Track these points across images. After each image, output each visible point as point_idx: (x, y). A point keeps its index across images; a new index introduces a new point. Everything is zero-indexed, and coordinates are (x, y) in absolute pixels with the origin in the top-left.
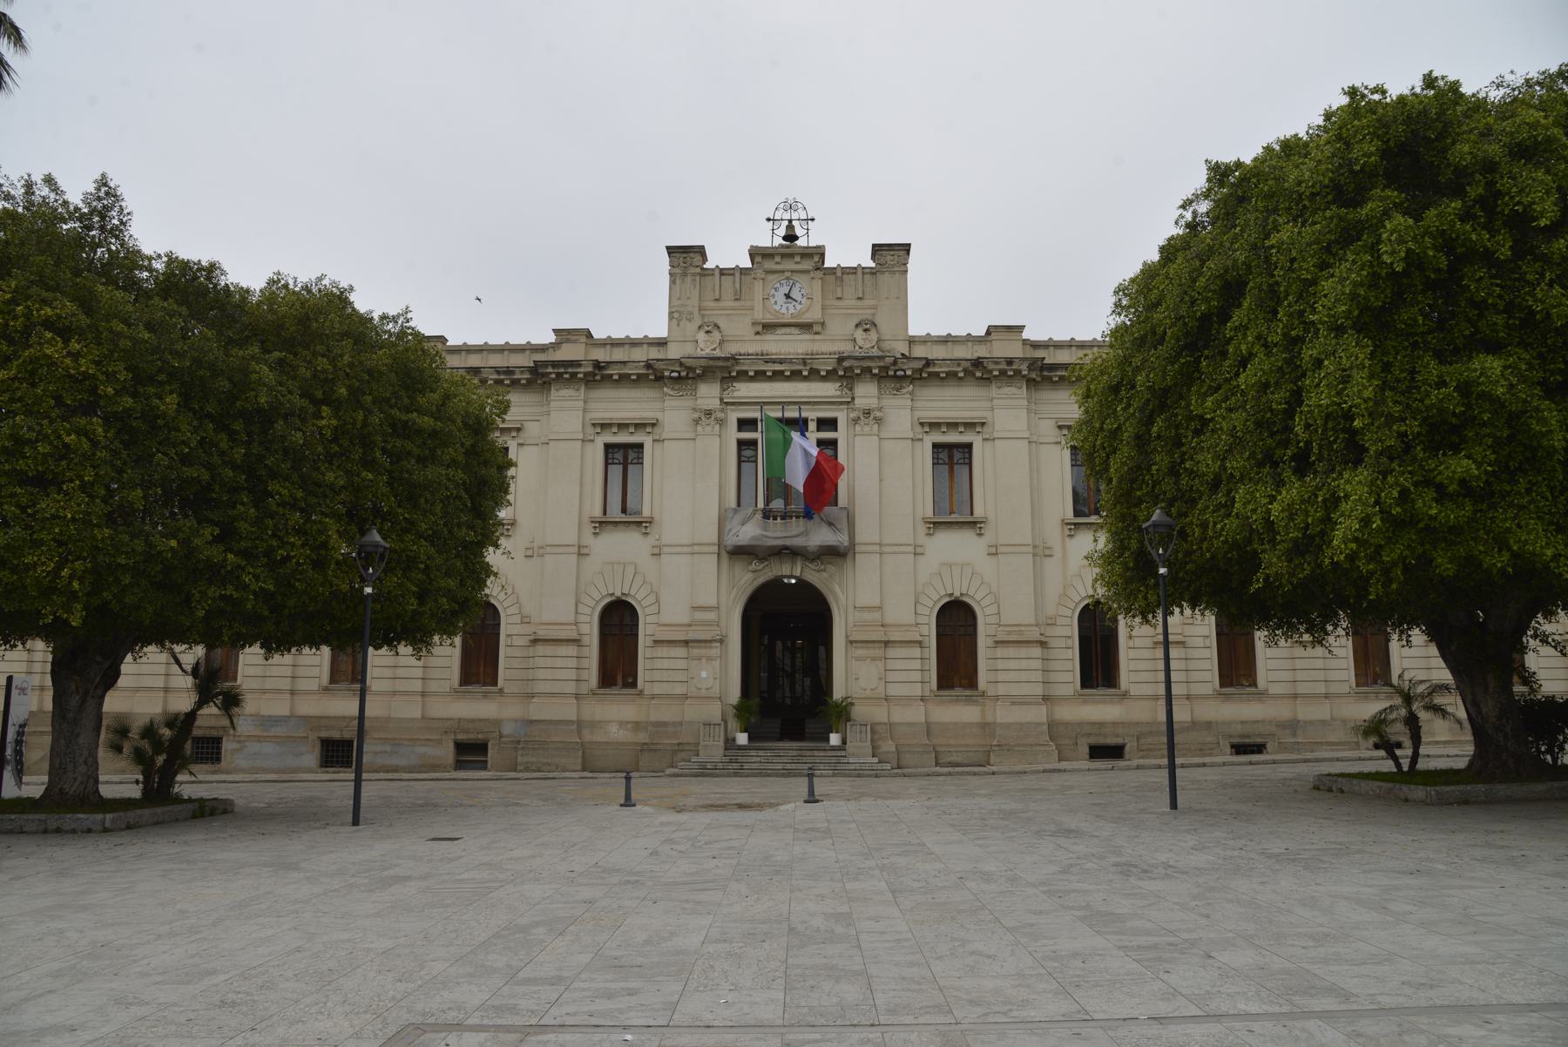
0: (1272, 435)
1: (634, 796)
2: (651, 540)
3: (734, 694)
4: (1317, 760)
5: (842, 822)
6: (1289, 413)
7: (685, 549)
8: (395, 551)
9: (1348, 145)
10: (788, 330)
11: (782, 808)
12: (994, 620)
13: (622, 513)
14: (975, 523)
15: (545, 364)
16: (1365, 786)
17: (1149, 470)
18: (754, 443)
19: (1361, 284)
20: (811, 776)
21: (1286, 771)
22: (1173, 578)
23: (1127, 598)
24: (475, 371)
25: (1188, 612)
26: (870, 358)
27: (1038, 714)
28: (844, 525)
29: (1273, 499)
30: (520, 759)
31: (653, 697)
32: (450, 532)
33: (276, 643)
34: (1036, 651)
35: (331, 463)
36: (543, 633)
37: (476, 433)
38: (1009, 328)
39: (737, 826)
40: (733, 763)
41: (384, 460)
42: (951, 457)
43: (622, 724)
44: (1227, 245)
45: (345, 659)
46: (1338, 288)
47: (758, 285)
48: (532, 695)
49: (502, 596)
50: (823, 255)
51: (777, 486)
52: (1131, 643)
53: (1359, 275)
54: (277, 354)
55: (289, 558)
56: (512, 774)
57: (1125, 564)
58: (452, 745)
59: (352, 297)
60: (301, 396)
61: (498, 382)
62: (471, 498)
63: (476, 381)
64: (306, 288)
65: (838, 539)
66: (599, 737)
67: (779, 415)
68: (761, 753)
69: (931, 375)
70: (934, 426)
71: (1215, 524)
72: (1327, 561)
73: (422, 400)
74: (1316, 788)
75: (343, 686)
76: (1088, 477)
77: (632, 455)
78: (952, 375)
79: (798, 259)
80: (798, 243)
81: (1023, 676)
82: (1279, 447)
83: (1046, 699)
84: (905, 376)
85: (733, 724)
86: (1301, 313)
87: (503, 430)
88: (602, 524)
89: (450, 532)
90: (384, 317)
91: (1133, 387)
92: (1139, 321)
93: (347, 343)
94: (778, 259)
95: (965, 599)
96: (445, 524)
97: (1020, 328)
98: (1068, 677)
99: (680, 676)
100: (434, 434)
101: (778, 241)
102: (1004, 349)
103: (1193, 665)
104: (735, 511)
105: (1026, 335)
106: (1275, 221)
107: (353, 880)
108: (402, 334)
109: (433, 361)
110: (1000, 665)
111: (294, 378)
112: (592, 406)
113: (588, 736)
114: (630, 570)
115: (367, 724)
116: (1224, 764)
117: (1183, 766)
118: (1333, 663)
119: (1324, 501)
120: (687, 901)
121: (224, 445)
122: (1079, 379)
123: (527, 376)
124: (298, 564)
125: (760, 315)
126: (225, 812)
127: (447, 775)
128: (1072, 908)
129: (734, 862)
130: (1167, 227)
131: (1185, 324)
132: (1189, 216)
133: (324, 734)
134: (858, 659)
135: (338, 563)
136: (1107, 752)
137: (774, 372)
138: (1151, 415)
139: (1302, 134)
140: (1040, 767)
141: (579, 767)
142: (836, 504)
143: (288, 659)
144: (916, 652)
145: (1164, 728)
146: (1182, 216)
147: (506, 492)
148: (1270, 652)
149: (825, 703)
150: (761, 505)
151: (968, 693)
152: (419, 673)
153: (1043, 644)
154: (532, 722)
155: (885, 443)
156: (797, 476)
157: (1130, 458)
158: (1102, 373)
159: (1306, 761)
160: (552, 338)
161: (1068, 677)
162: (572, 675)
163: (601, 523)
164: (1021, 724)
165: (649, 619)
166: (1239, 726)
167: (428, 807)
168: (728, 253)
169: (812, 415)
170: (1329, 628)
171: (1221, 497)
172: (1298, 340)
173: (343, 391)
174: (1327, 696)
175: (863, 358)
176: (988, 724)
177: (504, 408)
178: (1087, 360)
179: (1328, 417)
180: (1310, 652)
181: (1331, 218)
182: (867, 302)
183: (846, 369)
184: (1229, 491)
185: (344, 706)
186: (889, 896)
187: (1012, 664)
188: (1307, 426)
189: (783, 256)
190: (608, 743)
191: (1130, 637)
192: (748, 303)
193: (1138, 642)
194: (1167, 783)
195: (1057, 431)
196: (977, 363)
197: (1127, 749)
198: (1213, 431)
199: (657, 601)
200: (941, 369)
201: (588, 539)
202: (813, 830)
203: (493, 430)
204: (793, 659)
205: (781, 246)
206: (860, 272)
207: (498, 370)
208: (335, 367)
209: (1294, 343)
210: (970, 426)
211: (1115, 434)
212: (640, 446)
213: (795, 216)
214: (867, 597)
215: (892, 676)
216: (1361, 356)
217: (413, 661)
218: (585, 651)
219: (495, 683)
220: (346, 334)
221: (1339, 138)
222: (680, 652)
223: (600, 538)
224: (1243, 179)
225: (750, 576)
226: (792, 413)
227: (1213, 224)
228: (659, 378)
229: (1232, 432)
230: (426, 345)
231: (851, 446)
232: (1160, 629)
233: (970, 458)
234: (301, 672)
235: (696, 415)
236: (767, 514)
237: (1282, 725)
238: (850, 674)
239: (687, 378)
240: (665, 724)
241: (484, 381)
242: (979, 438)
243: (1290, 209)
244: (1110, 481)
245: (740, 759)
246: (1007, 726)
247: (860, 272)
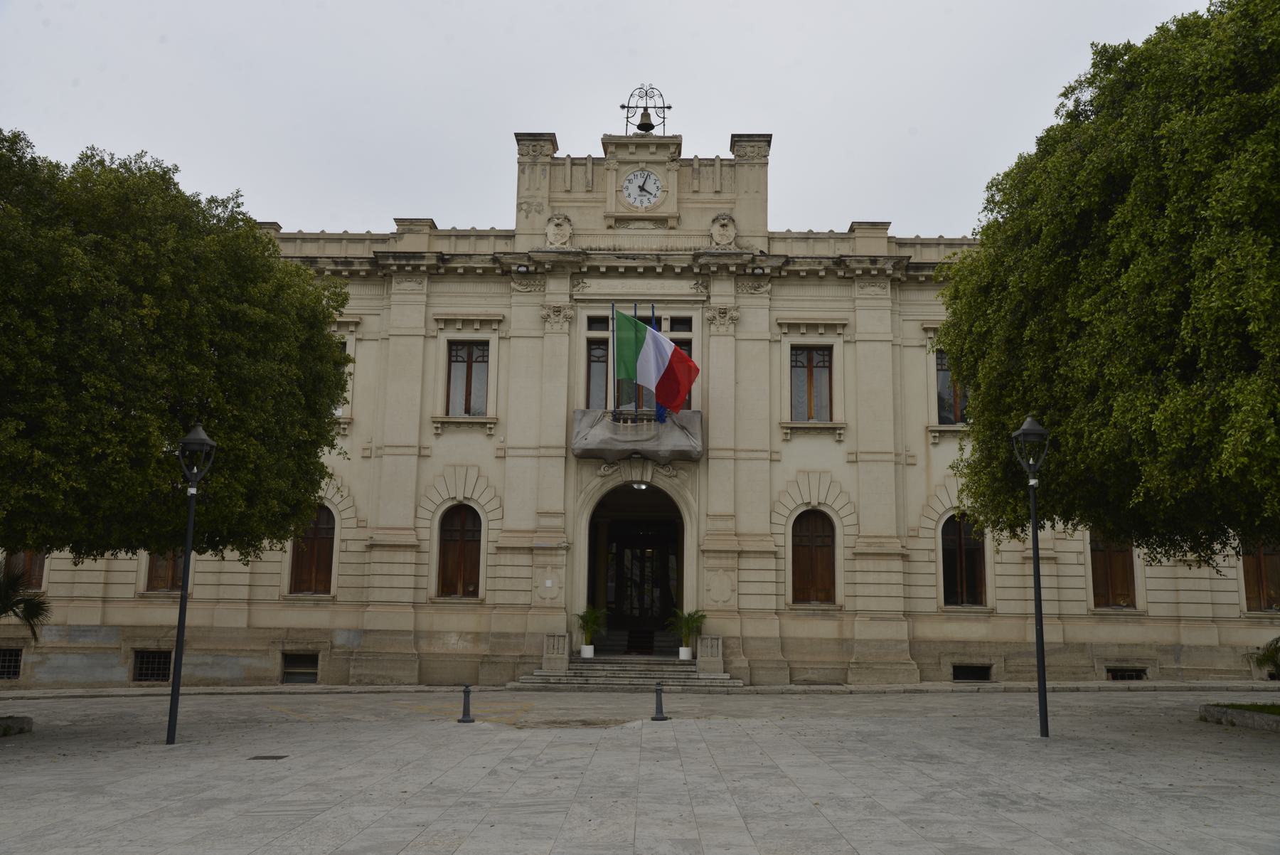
0: (1155, 339)
1: (473, 711)
2: (495, 442)
3: (581, 605)
4: (1203, 689)
5: (691, 741)
6: (1175, 317)
7: (531, 452)
8: (222, 450)
9: (1255, 22)
10: (641, 224)
11: (628, 725)
12: (853, 530)
13: (466, 414)
14: (835, 429)
15: (386, 255)
16: (1259, 719)
17: (1020, 375)
18: (604, 342)
19: (1262, 176)
20: (659, 692)
21: (1167, 700)
22: (1044, 489)
24: (311, 261)
25: (1060, 526)
27: (899, 631)
28: (697, 429)
29: (1154, 408)
30: (352, 671)
31: (495, 606)
32: (283, 430)
33: (85, 548)
34: (897, 565)
35: (152, 355)
36: (380, 538)
37: (312, 326)
38: (874, 225)
39: (581, 745)
40: (579, 676)
41: (212, 354)
42: (810, 360)
43: (461, 634)
44: (1112, 135)
46: (1232, 183)
47: (611, 176)
48: (367, 604)
49: (337, 499)
50: (679, 146)
51: (629, 389)
52: (998, 558)
53: (1259, 166)
54: (92, 236)
55: (104, 456)
57: (993, 474)
58: (279, 657)
59: (177, 178)
60: (120, 283)
61: (335, 273)
63: (312, 272)
64: (124, 165)
65: (689, 443)
66: (437, 649)
68: (607, 667)
69: (791, 273)
70: (793, 327)
71: (1091, 433)
72: (1214, 475)
73: (253, 291)
74: (1203, 719)
75: (163, 592)
76: (954, 382)
77: (476, 353)
78: (812, 274)
79: (653, 149)
81: (884, 590)
82: (1162, 352)
83: (908, 615)
84: (764, 275)
85: (578, 636)
86: (1192, 209)
87: (340, 324)
88: (444, 425)
89: (283, 430)
90: (212, 200)
91: (1005, 288)
92: (1013, 218)
93: (172, 227)
94: (632, 149)
95: (822, 508)
96: (277, 422)
97: (886, 225)
98: (931, 592)
99: (524, 585)
100: (266, 327)
101: (633, 130)
103: (1065, 582)
104: (584, 413)
105: (891, 232)
106: (1167, 108)
107: (165, 804)
108: (232, 219)
109: (265, 249)
110: (859, 578)
111: (112, 263)
112: (434, 300)
113: (424, 647)
114: (473, 474)
115: (187, 633)
116: (1100, 690)
117: (1054, 690)
118: (1222, 585)
119: (1212, 410)
120: (526, 825)
121: (31, 333)
122: (947, 279)
123: (367, 267)
124: (114, 462)
125: (612, 208)
126: (21, 731)
127: (272, 688)
128: (935, 840)
129: (577, 783)
130: (1047, 117)
131: (1063, 221)
132: (1070, 104)
133: (139, 645)
134: (710, 569)
135: (159, 461)
136: (972, 673)
137: (627, 269)
139: (1203, 12)
141: (415, 680)
142: (689, 408)
143: (101, 563)
144: (771, 563)
145: (1034, 648)
146: (1063, 105)
147: (343, 389)
148: (1149, 571)
149: (675, 615)
150: (611, 407)
151: (825, 606)
152: (246, 579)
153: (904, 557)
154: (366, 632)
155: (743, 345)
156: (649, 376)
157: (1000, 362)
158: (972, 273)
159: (1190, 689)
160: (393, 228)
161: (931, 592)
162: (410, 582)
163: (443, 423)
164: (880, 641)
165: (492, 525)
166: (1116, 649)
167: (250, 723)
168: (579, 142)
169: (665, 313)
170: (1217, 547)
171: (1097, 405)
172: (1188, 238)
173: (167, 278)
174: (1214, 620)
175: (720, 255)
176: (846, 640)
177: (343, 300)
178: (956, 260)
179: (1218, 321)
180: (1195, 571)
181: (1231, 105)
182: (725, 196)
183: (701, 267)
184: (1107, 400)
185: (164, 614)
186: (740, 822)
187: (872, 578)
188: (1195, 330)
189: (638, 146)
191: (998, 552)
192: (600, 196)
193: (1006, 557)
195: (922, 334)
196: (840, 261)
197: (994, 670)
198: (1090, 335)
201: (429, 440)
202: (660, 749)
203: (330, 324)
204: (642, 569)
205: (636, 135)
206: (718, 164)
207: (335, 261)
208: (158, 251)
209: (1182, 241)
210: (831, 327)
212: (485, 344)
215: (745, 588)
216: (1259, 255)
217: (240, 567)
218: (425, 558)
219: (328, 591)
220: (170, 218)
221: (1245, 14)
222: (524, 559)
223: (441, 438)
224: (1132, 64)
225: (597, 481)
226: (645, 312)
227: (1096, 113)
228: (507, 273)
229: (1112, 336)
230: (258, 232)
231: (705, 346)
232: (1029, 544)
234: (115, 578)
235: (544, 312)
236: (617, 417)
237: (1163, 649)
238: (701, 586)
239: (535, 273)
241: (320, 272)
243: (1184, 95)
244: (978, 387)
245: (586, 673)
246: (866, 643)
247: (718, 164)
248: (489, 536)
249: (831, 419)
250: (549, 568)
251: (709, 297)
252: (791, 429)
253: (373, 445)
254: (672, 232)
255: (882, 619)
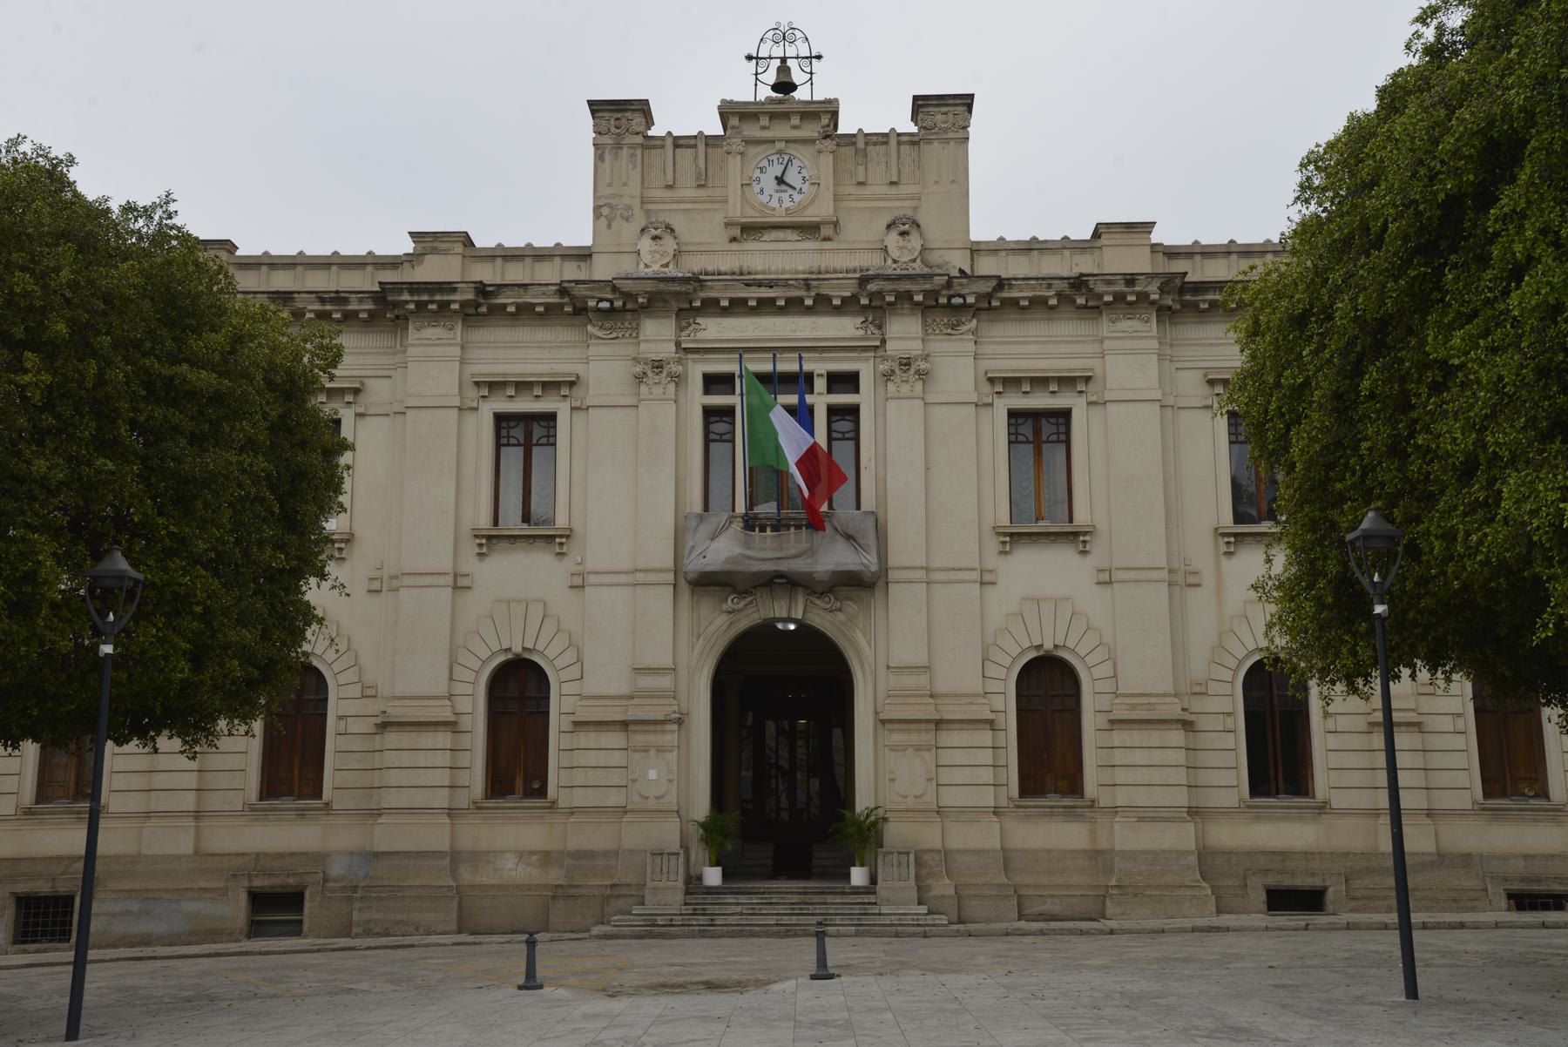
1: (541, 972)
2: (568, 564)
3: (701, 807)
5: (870, 1010)
7: (622, 578)
8: (153, 585)
10: (780, 234)
11: (776, 987)
12: (1108, 686)
13: (525, 523)
14: (1076, 534)
15: (398, 287)
17: (1356, 448)
18: (729, 412)
20: (820, 936)
23: (1323, 654)
24: (285, 297)
25: (1424, 675)
26: (911, 278)
27: (1181, 837)
30: (356, 916)
31: (572, 811)
32: (246, 554)
34: (1176, 737)
35: (41, 443)
36: (397, 712)
38: (1130, 227)
40: (699, 915)
41: (135, 441)
42: (1037, 432)
43: (522, 855)
44: (1494, 79)
45: (61, 758)
47: (734, 163)
48: (378, 813)
50: (835, 115)
51: (767, 476)
52: (1330, 724)
56: (343, 942)
57: (1319, 600)
58: (243, 899)
59: (73, 174)
62: (280, 501)
63: (285, 315)
66: (486, 877)
67: (767, 367)
68: (743, 899)
69: (1004, 301)
70: (1011, 383)
71: (1468, 534)
73: (196, 344)
76: (1256, 461)
78: (1038, 303)
79: (795, 121)
80: (797, 95)
81: (1157, 776)
83: (1194, 812)
84: (965, 306)
85: (698, 853)
87: (332, 393)
88: (492, 540)
89: (246, 554)
90: (129, 208)
91: (1330, 318)
93: (66, 249)
94: (764, 121)
96: (238, 542)
97: (1149, 226)
98: (1228, 778)
99: (616, 778)
100: (218, 398)
101: (765, 93)
102: (1123, 260)
103: (1436, 760)
104: (701, 518)
105: (1156, 237)
108: (161, 236)
109: (213, 280)
110: (1119, 757)
113: (467, 876)
115: (99, 867)
116: (1497, 925)
117: (1425, 926)
122: (1241, 305)
123: (370, 306)
125: (736, 211)
130: (1392, 55)
131: (1418, 214)
132: (1429, 34)
133: (23, 888)
134: (894, 748)
135: (54, 606)
136: (1296, 900)
137: (760, 301)
138: (1359, 361)
140: (1186, 923)
141: (454, 928)
144: (986, 737)
145: (1390, 862)
146: (1417, 35)
147: (338, 490)
150: (741, 508)
151: (1068, 802)
152: (191, 780)
153: (1187, 725)
154: (377, 855)
155: (937, 412)
158: (1279, 296)
160: (408, 246)
161: (1228, 778)
162: (444, 778)
163: (489, 538)
164: (1155, 852)
165: (566, 689)
166: (1521, 863)
168: (686, 112)
169: (819, 367)
171: (1477, 491)
173: (62, 327)
175: (899, 278)
177: (334, 357)
178: (1254, 275)
182: (906, 189)
183: (871, 296)
184: (1491, 482)
185: (62, 838)
187: (1138, 757)
189: (773, 116)
190: (498, 886)
191: (1326, 715)
192: (718, 192)
193: (1342, 723)
194: (1399, 953)
195: (1207, 389)
196: (1079, 283)
197: (1330, 896)
198: (1463, 385)
199: (579, 660)
200: (1021, 293)
201: (470, 563)
202: (825, 1023)
203: (314, 392)
204: (792, 750)
205: (770, 100)
207: (321, 297)
208: (45, 287)
210: (1067, 382)
211: (1300, 391)
212: (551, 417)
213: (791, 52)
214: (907, 650)
215: (947, 776)
217: (183, 762)
218: (465, 740)
219: (318, 794)
220: (64, 235)
222: (615, 739)
223: (487, 560)
225: (723, 619)
226: (788, 365)
227: (1469, 45)
228: (580, 311)
229: (1497, 385)
230: (202, 256)
231: (880, 415)
232: (1377, 701)
233: (1068, 433)
235: (638, 369)
236: (750, 523)
238: (881, 773)
239: (624, 310)
240: (590, 855)
241: (298, 315)
242: (1082, 401)
245: (710, 909)
248: (561, 706)
249: (1071, 520)
250: (652, 752)
251: (883, 341)
252: (1012, 535)
253: (385, 574)
254: (827, 245)
255: (1154, 820)
